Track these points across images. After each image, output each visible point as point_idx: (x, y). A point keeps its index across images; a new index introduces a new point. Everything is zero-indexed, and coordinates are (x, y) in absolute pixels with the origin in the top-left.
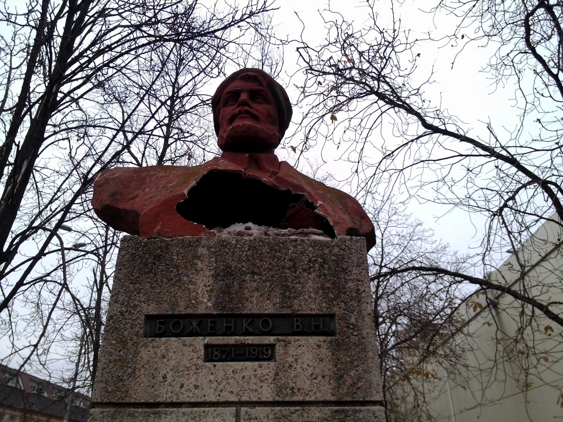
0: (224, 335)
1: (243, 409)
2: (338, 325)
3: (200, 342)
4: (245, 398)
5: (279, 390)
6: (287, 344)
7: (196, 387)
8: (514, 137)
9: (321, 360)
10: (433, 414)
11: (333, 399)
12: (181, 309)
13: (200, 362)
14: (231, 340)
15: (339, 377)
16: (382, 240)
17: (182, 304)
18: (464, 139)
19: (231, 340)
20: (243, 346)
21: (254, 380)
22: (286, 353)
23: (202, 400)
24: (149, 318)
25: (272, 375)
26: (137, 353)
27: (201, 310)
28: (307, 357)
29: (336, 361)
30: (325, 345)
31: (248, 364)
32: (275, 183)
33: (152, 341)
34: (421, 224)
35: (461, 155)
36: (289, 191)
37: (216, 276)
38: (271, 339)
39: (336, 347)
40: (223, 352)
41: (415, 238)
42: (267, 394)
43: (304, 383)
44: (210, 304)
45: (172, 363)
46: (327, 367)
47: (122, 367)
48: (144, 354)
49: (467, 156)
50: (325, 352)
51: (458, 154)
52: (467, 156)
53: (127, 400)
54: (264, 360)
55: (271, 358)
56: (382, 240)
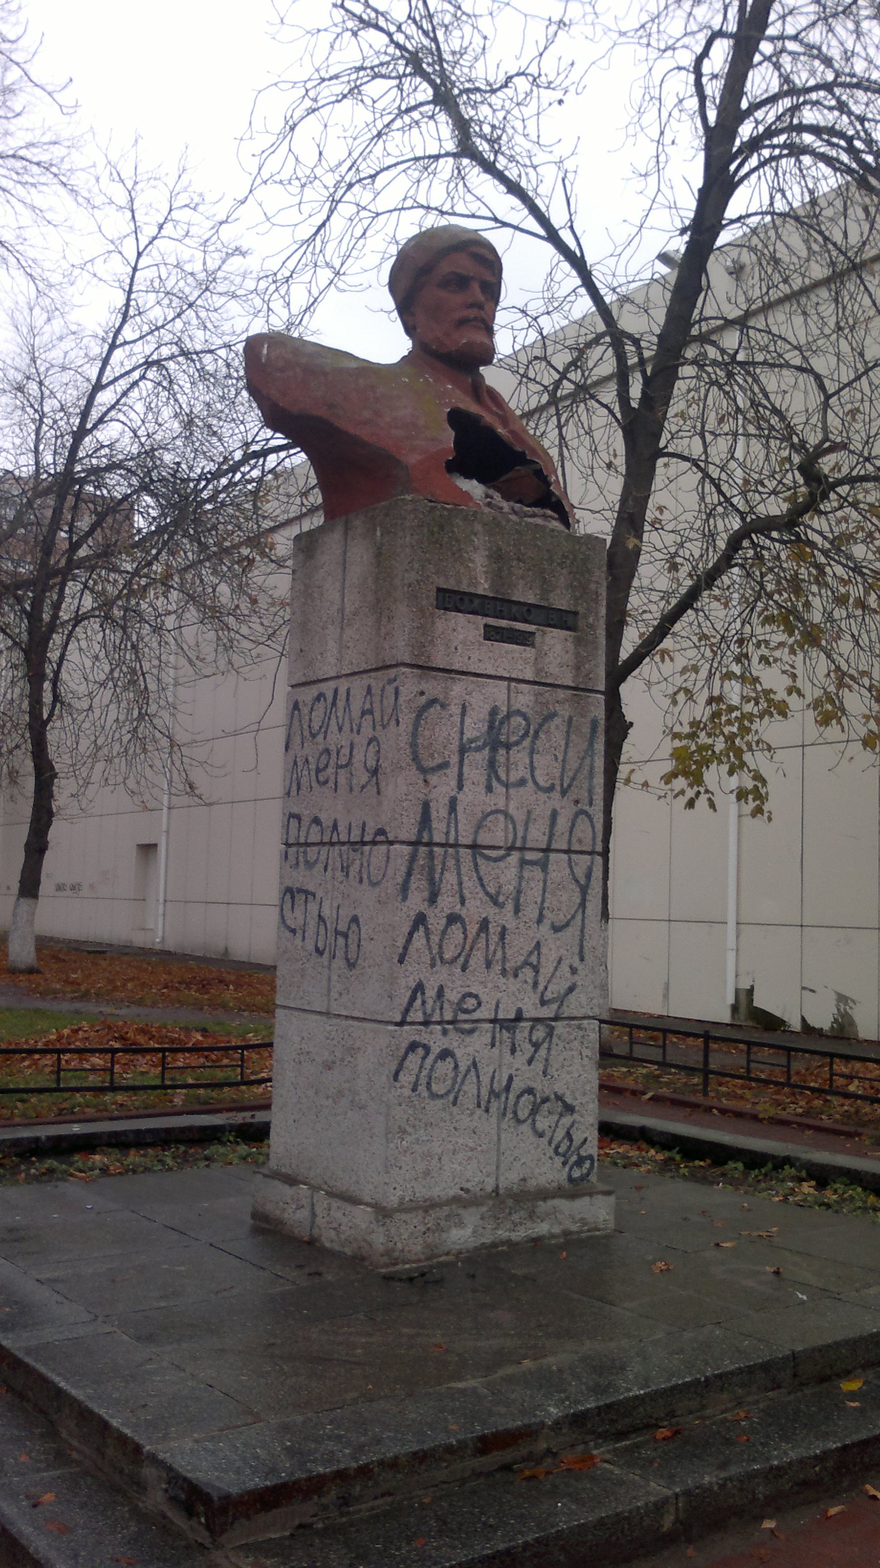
0: (497, 617)
1: (513, 684)
2: (581, 623)
3: (481, 621)
4: (513, 676)
5: (538, 671)
6: (544, 633)
7: (480, 661)
8: (617, 252)
9: (567, 652)
10: (181, 737)
11: (572, 685)
12: (464, 587)
13: (482, 640)
14: (504, 623)
15: (578, 668)
16: (135, 269)
17: (465, 582)
18: (514, 188)
19: (504, 623)
20: (511, 630)
21: (520, 662)
22: (543, 642)
23: (485, 672)
24: (439, 590)
25: (533, 658)
26: (433, 623)
27: (480, 591)
28: (558, 648)
29: (577, 655)
30: (571, 640)
31: (515, 646)
32: (512, 439)
33: (444, 614)
34: (243, 254)
35: (496, 219)
36: (523, 453)
37: (489, 557)
38: (531, 628)
39: (578, 642)
40: (497, 633)
41: (221, 288)
42: (529, 675)
43: (554, 669)
44: (486, 586)
45: (461, 637)
46: (569, 658)
47: (423, 634)
48: (440, 625)
49: (505, 224)
50: (570, 646)
51: (490, 215)
52: (505, 224)
53: (430, 664)
54: (528, 645)
55: (532, 645)
56: (135, 269)
